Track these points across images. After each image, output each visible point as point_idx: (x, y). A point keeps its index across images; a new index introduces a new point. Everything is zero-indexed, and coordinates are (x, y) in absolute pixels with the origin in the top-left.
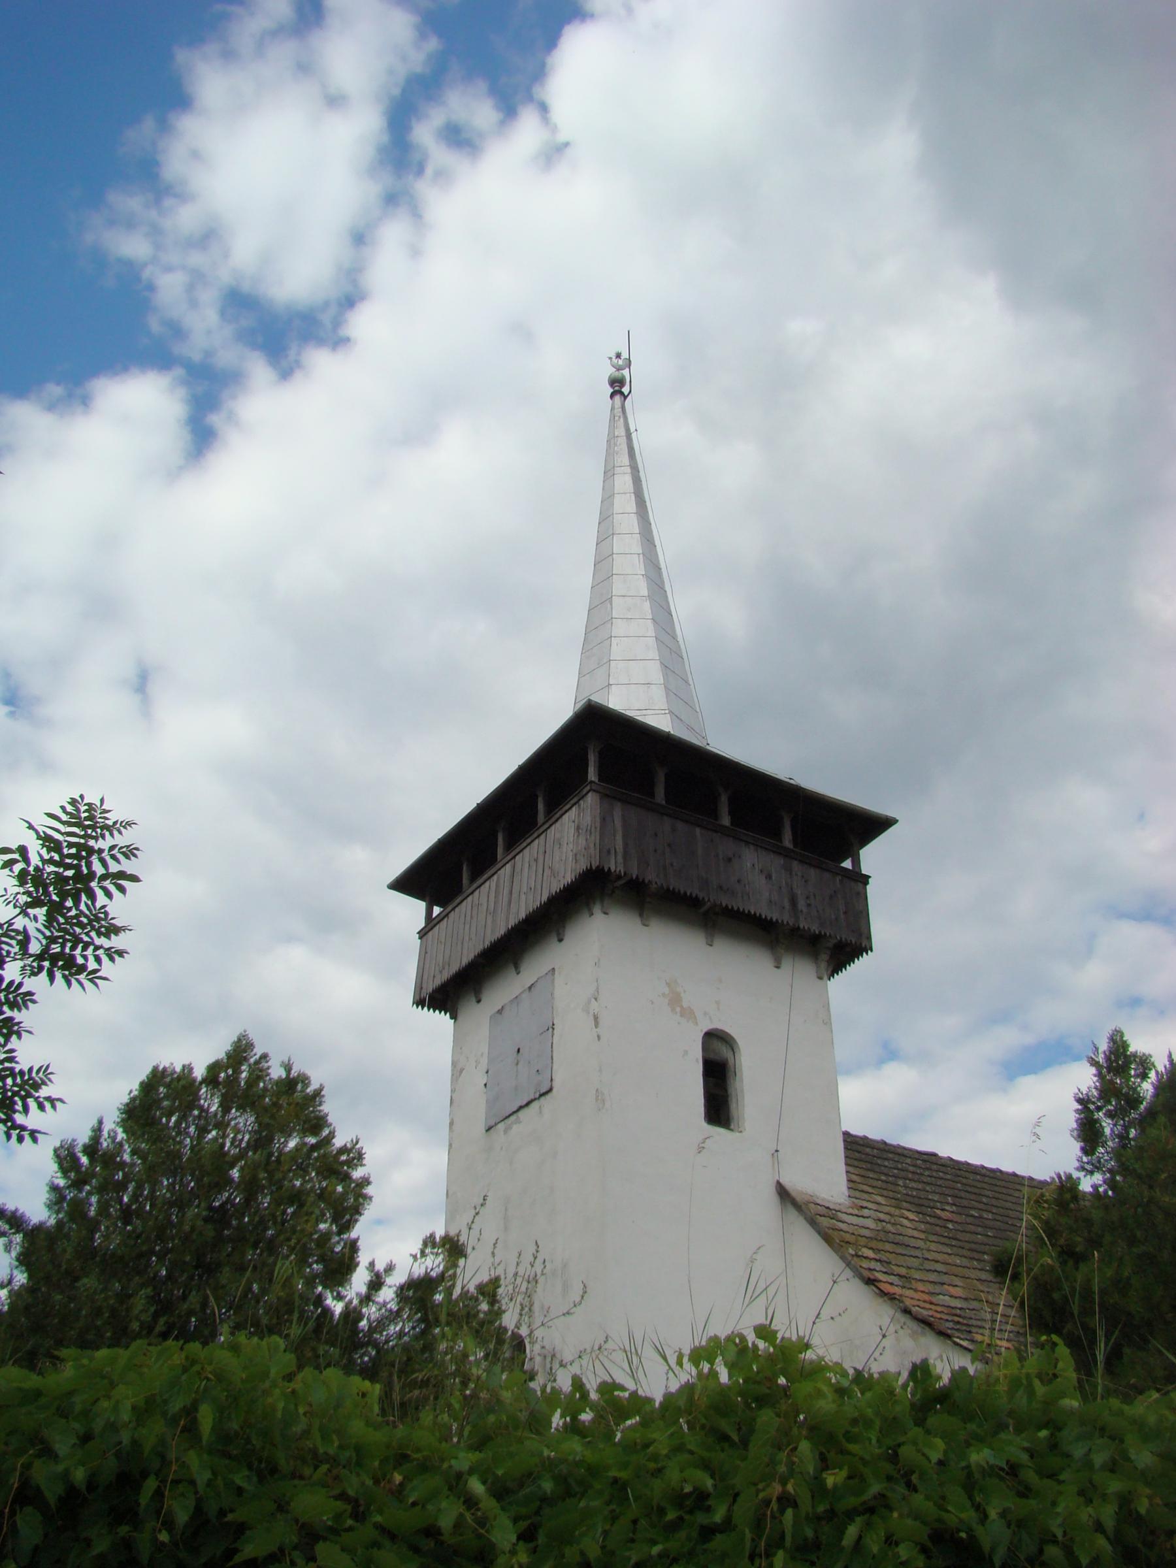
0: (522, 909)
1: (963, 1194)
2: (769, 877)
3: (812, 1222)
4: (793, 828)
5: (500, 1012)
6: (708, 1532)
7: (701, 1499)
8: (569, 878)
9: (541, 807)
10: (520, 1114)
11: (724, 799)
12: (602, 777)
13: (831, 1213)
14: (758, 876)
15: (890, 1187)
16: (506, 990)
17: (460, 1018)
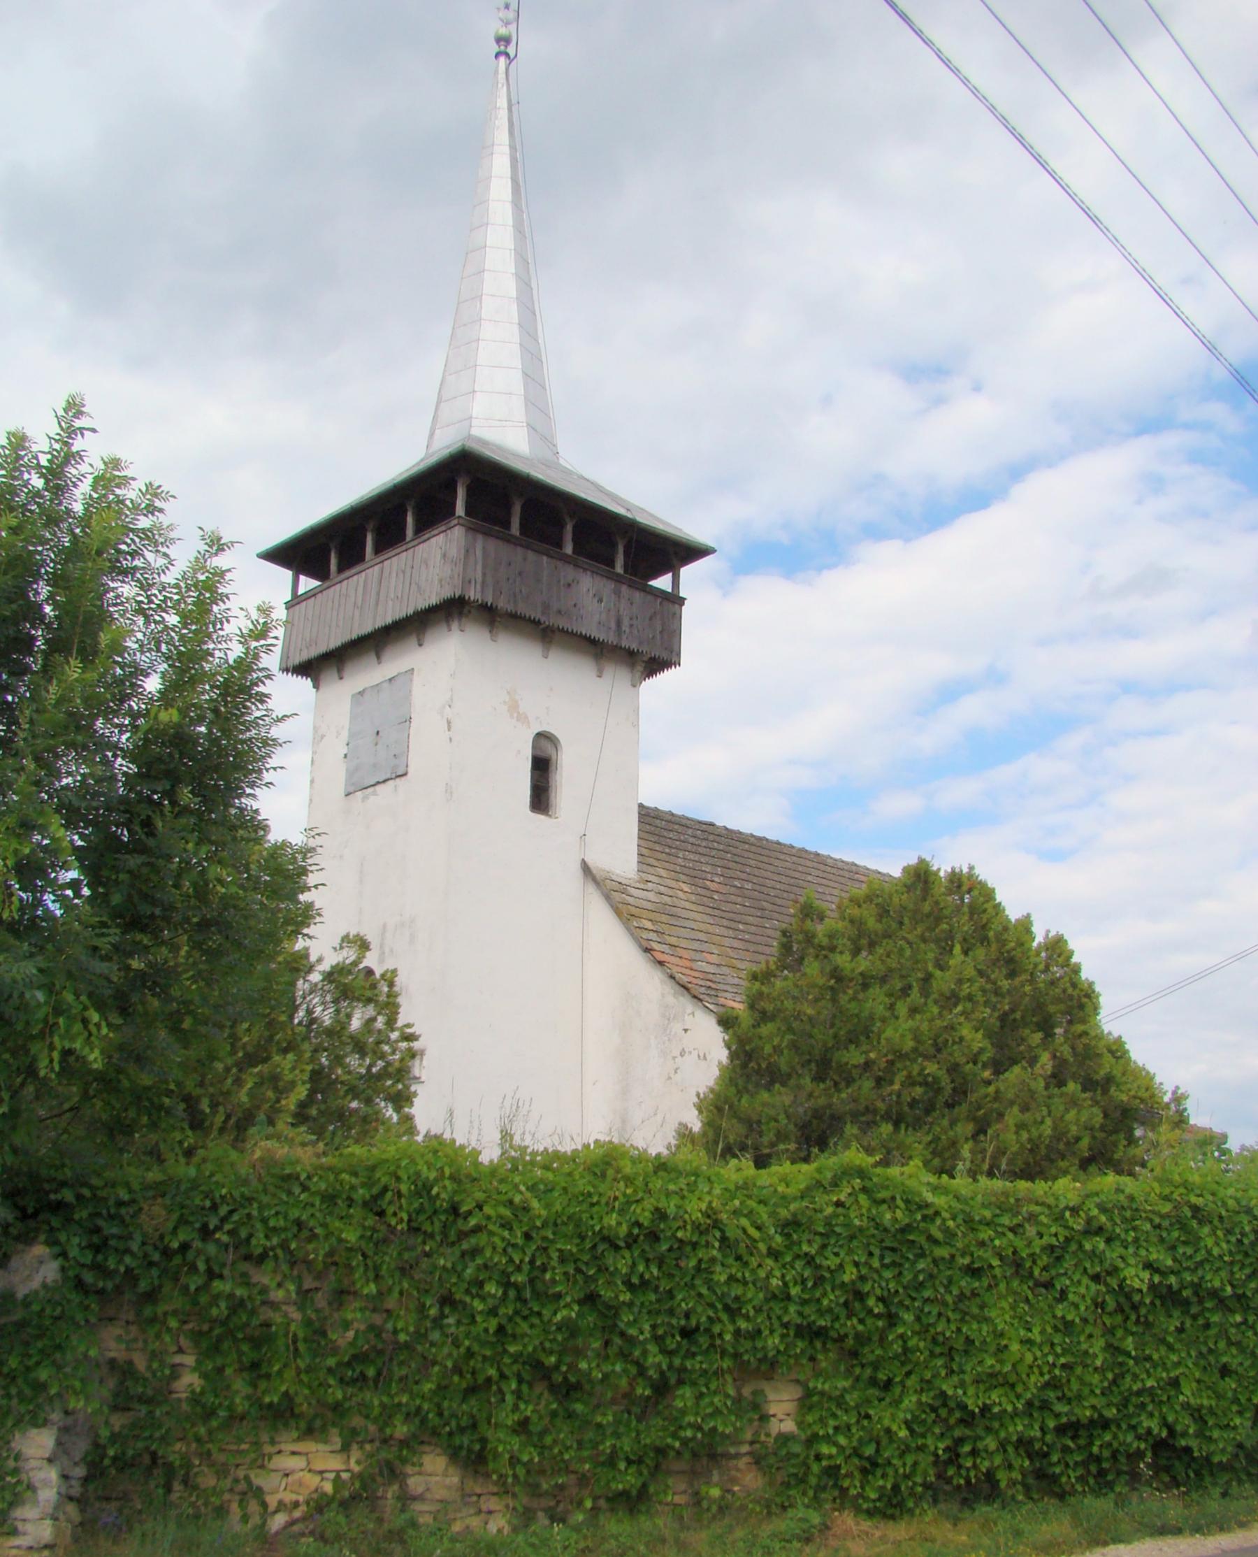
0: (389, 615)
1: (731, 865)
2: (600, 601)
3: (607, 897)
4: (626, 554)
5: (361, 693)
6: (593, 1205)
7: (590, 1195)
8: (434, 600)
9: (410, 520)
10: (378, 788)
11: (569, 528)
12: (469, 512)
13: (622, 888)
14: (591, 598)
15: (672, 859)
16: (367, 675)
17: (322, 689)
